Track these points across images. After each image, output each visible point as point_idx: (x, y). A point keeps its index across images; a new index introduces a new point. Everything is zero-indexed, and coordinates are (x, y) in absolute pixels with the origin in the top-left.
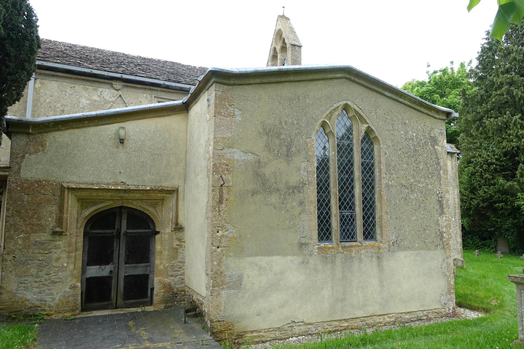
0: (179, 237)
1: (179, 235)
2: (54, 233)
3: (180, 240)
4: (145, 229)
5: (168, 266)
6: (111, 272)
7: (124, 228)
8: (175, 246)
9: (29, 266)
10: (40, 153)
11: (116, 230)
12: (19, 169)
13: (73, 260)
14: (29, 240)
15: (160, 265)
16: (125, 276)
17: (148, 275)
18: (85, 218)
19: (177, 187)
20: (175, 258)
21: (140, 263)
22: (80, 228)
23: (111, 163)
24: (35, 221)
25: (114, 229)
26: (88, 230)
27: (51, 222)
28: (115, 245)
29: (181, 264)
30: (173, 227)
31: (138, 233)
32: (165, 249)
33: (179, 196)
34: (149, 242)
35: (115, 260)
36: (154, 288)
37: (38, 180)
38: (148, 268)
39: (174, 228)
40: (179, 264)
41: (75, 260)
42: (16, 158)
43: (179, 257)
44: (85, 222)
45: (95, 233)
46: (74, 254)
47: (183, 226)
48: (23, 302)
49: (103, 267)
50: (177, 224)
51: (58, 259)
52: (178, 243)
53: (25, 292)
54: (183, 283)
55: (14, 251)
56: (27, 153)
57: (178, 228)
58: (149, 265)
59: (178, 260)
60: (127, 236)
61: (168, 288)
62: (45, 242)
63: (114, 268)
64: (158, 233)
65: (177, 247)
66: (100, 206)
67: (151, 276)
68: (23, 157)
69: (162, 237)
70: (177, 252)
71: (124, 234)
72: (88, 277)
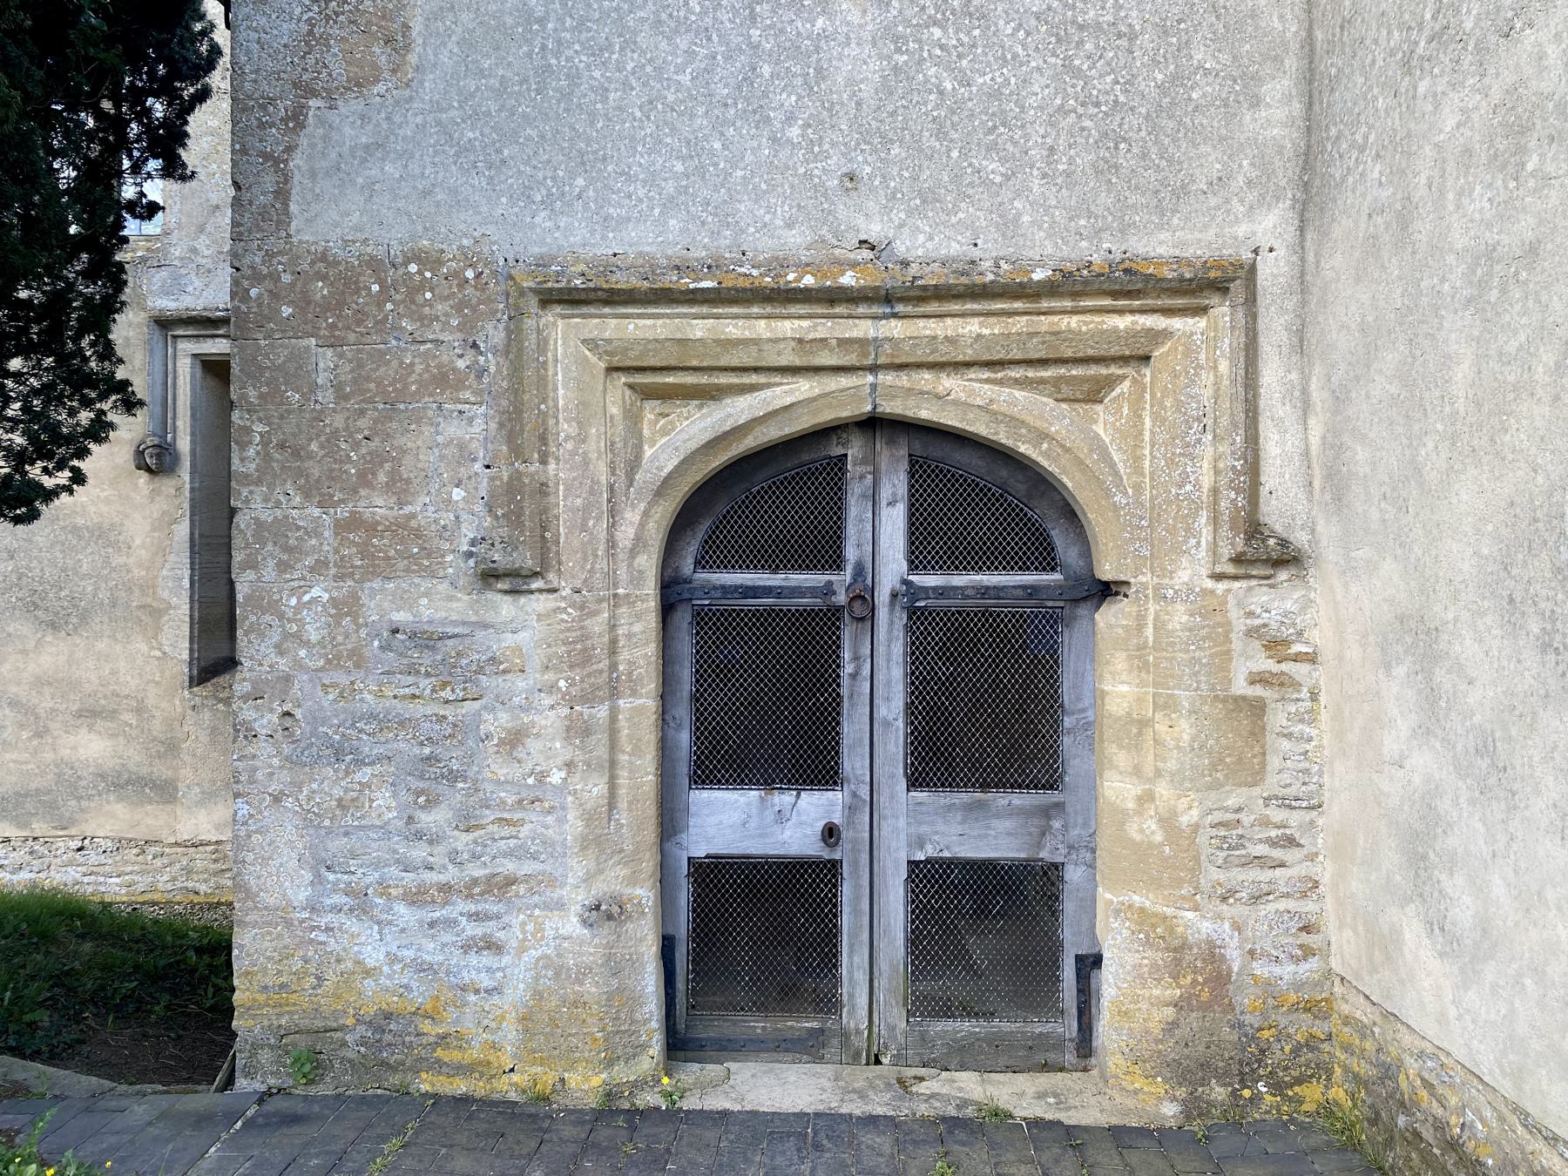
0: (1272, 618)
1: (1272, 602)
2: (489, 576)
3: (1275, 646)
4: (1025, 568)
5: (1195, 828)
6: (830, 833)
7: (893, 566)
8: (1240, 687)
9: (364, 775)
10: (380, 88)
11: (848, 575)
12: (282, 194)
13: (602, 752)
14: (355, 617)
15: (1139, 812)
16: (913, 865)
17: (1056, 867)
18: (661, 490)
19: (1247, 256)
20: (1245, 763)
21: (1002, 784)
22: (633, 553)
23: (790, 119)
24: (379, 506)
25: (837, 563)
26: (687, 566)
27: (458, 509)
28: (849, 669)
29: (1295, 818)
30: (1226, 552)
31: (984, 591)
32: (1166, 705)
33: (1262, 324)
34: (1054, 652)
35: (853, 762)
36: (1097, 961)
37: (380, 252)
38: (1057, 824)
39: (1238, 560)
40: (1277, 815)
41: (613, 746)
42: (262, 126)
43: (1274, 762)
44: (665, 511)
45: (726, 590)
46: (602, 712)
47: (1300, 538)
48: (347, 978)
49: (784, 799)
50: (1254, 529)
51: (514, 740)
52: (1265, 663)
53: (352, 925)
54: (1308, 952)
55: (287, 679)
56: (314, 94)
57: (1265, 554)
58: (1059, 806)
59: (1272, 784)
60: (912, 612)
61: (1206, 977)
62: (450, 630)
63: (851, 809)
64: (1107, 591)
65: (1258, 691)
66: (740, 409)
67: (1073, 875)
68: (297, 118)
69: (1141, 618)
70: (1257, 732)
71: (894, 595)
72: (700, 852)
